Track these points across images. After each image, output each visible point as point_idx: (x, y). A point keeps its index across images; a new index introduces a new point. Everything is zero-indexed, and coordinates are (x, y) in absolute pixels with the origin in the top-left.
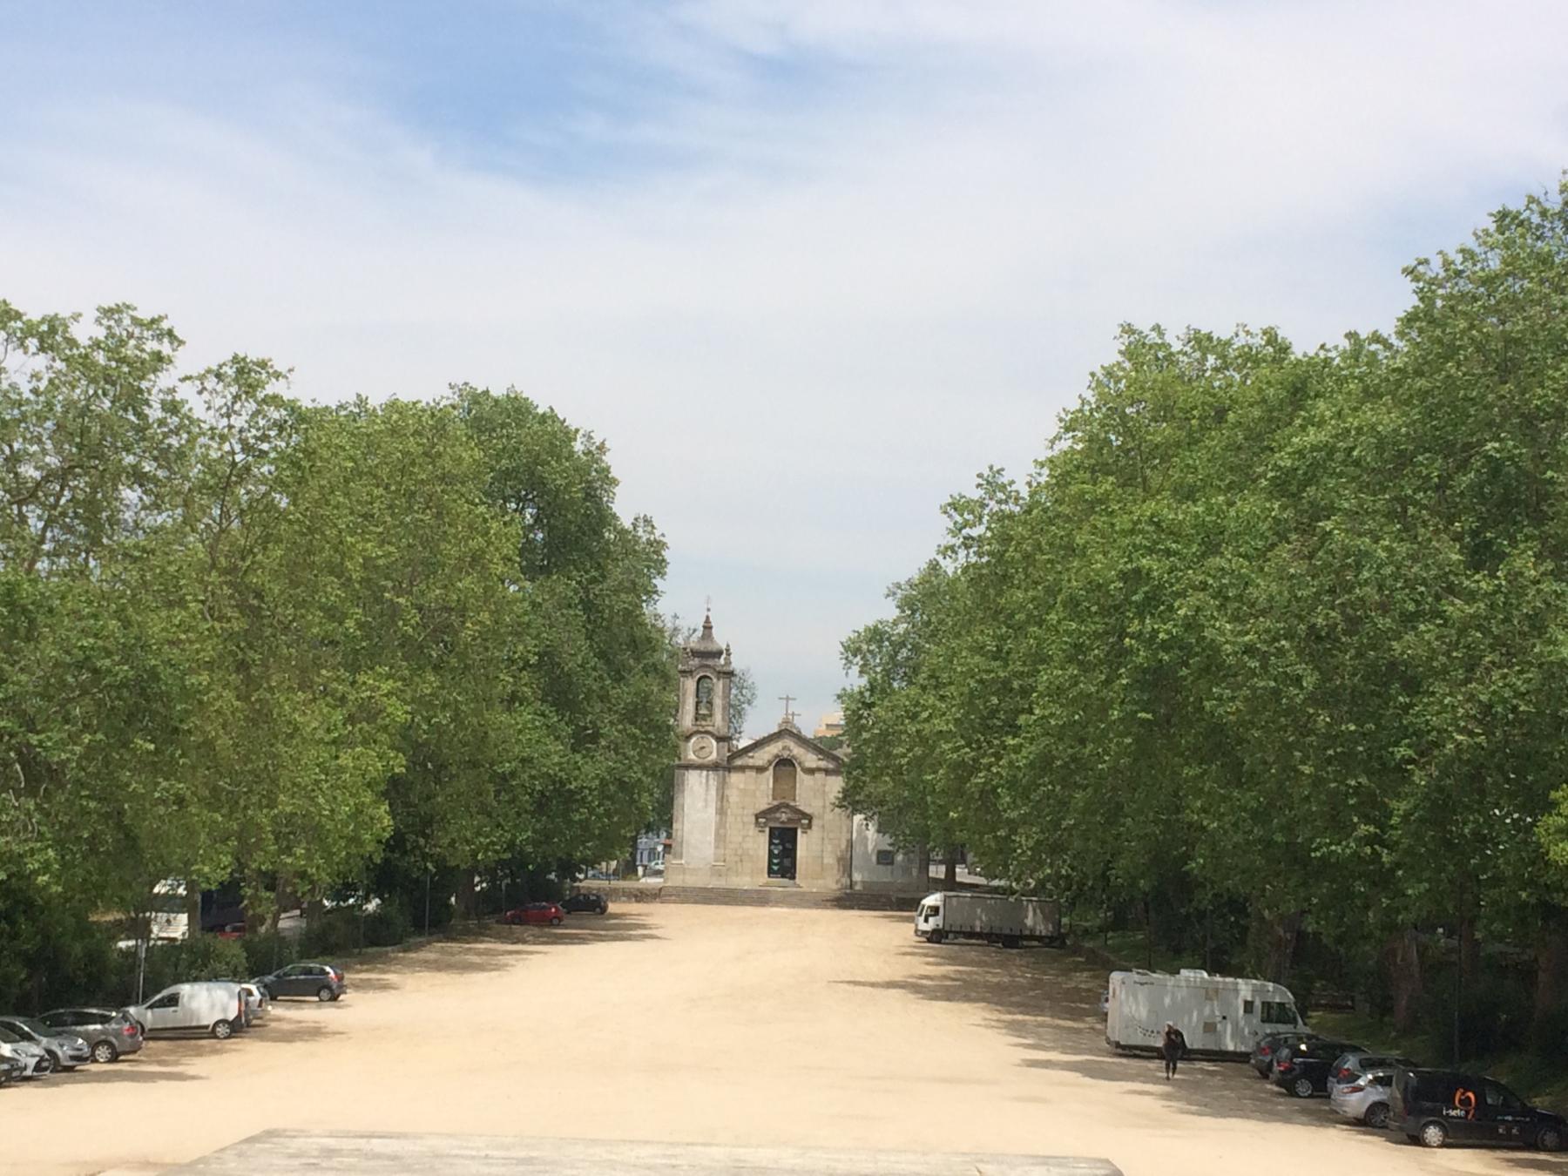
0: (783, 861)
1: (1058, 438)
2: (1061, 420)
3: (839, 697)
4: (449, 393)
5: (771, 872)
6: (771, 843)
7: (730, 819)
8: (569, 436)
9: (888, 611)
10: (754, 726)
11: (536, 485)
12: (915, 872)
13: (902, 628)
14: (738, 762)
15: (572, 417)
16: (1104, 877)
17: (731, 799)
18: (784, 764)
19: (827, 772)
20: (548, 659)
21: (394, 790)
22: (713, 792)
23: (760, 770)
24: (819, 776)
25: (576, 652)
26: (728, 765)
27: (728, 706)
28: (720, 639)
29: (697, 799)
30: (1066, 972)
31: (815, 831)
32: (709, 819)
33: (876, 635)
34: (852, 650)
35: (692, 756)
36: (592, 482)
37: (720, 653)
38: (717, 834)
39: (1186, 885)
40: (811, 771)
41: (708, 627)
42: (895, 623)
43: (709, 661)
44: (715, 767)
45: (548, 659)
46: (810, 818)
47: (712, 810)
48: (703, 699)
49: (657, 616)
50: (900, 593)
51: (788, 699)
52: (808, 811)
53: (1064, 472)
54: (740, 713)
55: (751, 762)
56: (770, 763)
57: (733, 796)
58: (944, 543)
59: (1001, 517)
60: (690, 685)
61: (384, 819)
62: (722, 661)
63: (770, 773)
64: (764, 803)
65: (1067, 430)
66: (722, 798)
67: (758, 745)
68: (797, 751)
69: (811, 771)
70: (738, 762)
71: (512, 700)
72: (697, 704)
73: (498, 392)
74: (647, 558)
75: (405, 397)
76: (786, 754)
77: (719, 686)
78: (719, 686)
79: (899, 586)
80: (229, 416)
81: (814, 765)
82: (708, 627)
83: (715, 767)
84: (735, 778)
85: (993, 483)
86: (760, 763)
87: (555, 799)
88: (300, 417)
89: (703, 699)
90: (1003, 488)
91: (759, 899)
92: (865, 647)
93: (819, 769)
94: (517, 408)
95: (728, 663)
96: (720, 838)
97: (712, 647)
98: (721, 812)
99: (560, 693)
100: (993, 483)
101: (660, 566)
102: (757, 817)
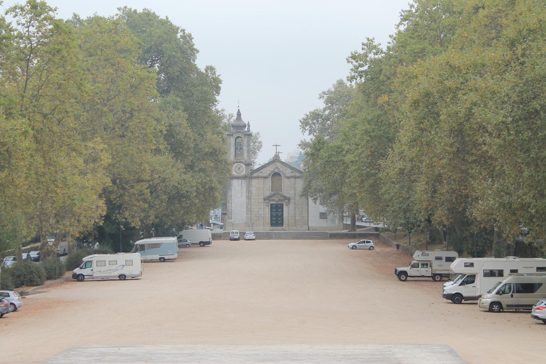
0: (277, 218)
1: (400, 24)
2: (401, 15)
3: (300, 145)
4: (118, 12)
5: (272, 224)
6: (271, 211)
7: (253, 201)
8: (174, 30)
9: (320, 105)
10: (262, 158)
11: (160, 53)
12: (337, 221)
13: (327, 112)
14: (255, 175)
15: (175, 22)
16: (429, 221)
17: (253, 192)
18: (276, 175)
19: (295, 177)
20: (169, 134)
21: (105, 193)
22: (245, 189)
23: (265, 178)
24: (292, 180)
25: (184, 129)
26: (250, 176)
27: (249, 151)
28: (245, 119)
29: (238, 193)
30: (32, 238)
31: (292, 205)
32: (242, 200)
33: (315, 115)
34: (305, 123)
35: (234, 173)
36: (186, 49)
37: (245, 126)
38: (247, 208)
39: (466, 223)
40: (289, 178)
41: (239, 114)
42: (325, 110)
43: (240, 129)
44: (245, 177)
45: (169, 134)
46: (289, 199)
47: (244, 198)
48: (238, 148)
49: (217, 112)
50: (325, 96)
51: (276, 146)
52: (288, 196)
53: (401, 42)
54: (255, 153)
55: (261, 175)
56: (270, 175)
57: (254, 190)
58: (349, 75)
59: (373, 62)
60: (232, 140)
61: (103, 210)
62: (246, 129)
63: (269, 180)
64: (268, 193)
65: (405, 20)
66: (249, 191)
67: (263, 167)
68: (282, 169)
69: (289, 178)
70: (255, 175)
71: (158, 151)
72: (236, 149)
73: (140, 10)
74: (210, 84)
75: (100, 14)
76: (276, 171)
77: (245, 140)
78: (245, 140)
79: (324, 93)
80: (28, 27)
81: (289, 175)
82: (239, 114)
83: (245, 177)
84: (254, 182)
85: (370, 46)
86: (265, 175)
87: (177, 196)
88: (58, 26)
89: (238, 148)
90: (375, 47)
91: (267, 236)
92: (310, 122)
93: (292, 177)
94: (148, 17)
95: (249, 130)
96: (249, 210)
97: (241, 124)
98: (249, 198)
99: (177, 148)
100: (370, 46)
101: (218, 90)
102: (265, 199)
